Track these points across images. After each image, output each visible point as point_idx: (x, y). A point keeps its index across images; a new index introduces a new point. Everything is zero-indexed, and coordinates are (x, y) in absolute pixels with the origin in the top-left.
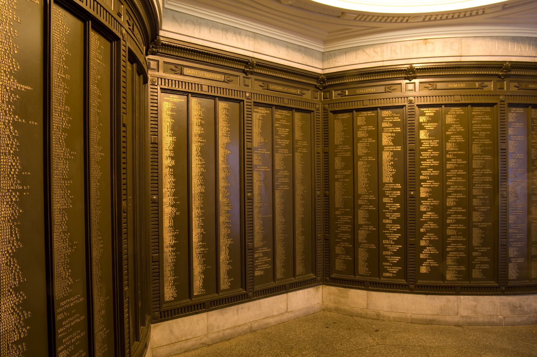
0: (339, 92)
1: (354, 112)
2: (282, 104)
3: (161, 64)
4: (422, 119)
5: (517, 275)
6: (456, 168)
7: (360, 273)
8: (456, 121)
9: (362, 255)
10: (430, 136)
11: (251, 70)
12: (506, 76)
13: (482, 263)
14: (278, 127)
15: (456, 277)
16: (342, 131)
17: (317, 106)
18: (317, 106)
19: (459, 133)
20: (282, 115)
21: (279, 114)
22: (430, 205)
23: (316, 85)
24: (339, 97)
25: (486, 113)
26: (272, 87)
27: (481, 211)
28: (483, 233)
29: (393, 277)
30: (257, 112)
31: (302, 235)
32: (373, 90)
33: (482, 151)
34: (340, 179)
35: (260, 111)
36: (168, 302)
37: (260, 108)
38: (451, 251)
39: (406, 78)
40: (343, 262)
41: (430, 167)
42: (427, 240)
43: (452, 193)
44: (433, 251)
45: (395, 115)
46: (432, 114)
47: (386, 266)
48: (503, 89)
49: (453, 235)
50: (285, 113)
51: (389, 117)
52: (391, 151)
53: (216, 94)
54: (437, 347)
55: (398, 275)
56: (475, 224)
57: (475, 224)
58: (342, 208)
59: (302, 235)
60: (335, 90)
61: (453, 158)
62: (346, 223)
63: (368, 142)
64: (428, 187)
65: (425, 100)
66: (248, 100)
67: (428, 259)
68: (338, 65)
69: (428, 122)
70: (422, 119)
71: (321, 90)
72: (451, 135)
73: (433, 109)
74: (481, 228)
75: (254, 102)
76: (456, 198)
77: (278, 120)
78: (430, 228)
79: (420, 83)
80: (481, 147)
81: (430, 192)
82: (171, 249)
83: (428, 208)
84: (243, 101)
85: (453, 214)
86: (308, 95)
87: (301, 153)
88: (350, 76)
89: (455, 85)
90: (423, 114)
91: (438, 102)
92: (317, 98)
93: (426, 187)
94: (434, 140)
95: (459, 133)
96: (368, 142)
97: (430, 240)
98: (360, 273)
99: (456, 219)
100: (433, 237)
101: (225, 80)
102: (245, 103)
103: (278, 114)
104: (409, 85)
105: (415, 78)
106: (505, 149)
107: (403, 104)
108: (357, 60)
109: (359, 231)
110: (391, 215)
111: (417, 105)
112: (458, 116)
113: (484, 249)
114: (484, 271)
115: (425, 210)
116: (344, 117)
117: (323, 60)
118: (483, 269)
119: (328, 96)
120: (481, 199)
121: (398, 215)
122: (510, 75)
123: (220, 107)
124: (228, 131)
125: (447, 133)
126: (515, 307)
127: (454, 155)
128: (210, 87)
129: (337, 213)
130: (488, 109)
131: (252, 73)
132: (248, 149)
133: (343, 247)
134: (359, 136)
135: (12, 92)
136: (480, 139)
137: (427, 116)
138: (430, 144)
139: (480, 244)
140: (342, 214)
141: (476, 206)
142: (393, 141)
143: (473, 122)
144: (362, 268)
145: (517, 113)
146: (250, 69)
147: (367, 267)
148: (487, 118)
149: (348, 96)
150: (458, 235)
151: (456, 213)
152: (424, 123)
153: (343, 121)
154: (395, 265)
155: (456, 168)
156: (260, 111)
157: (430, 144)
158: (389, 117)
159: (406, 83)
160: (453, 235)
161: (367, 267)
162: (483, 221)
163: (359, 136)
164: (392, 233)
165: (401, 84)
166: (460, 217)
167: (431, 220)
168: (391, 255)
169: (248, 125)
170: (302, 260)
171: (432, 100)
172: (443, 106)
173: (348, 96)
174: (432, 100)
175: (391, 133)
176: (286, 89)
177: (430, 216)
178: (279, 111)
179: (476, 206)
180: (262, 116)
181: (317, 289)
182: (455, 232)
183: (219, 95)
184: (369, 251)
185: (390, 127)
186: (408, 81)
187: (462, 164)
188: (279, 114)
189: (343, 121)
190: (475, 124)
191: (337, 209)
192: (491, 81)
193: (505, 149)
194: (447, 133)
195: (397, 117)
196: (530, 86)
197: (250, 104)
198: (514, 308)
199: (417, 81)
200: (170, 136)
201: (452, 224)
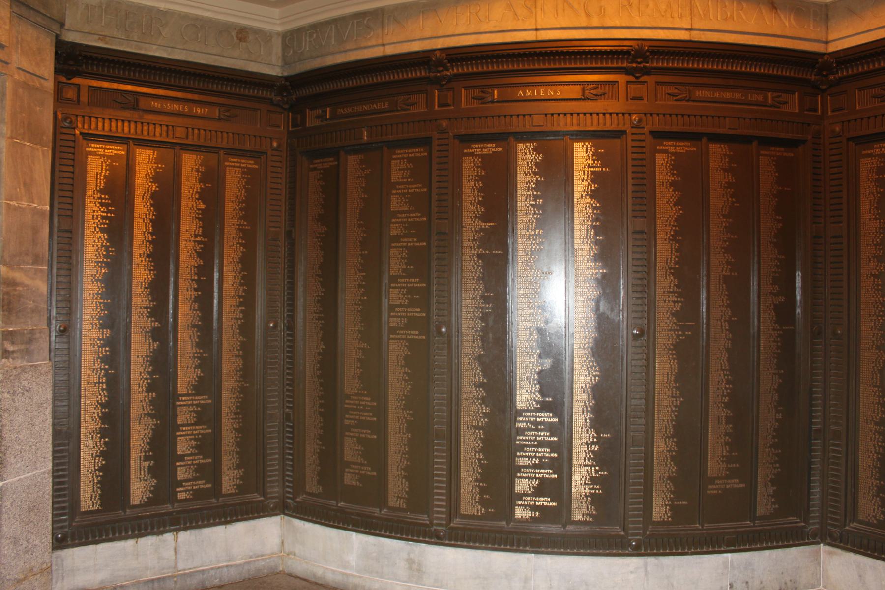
0: (477, 93)
7: (463, 512)
24: (476, 105)
32: (542, 93)
36: (135, 506)
48: (816, 110)
60: (466, 88)
82: (872, 426)
88: (483, 58)
89: (728, 95)
91: (614, 127)
98: (463, 512)
107: (623, 129)
119: (450, 101)
122: (841, 79)
131: (648, 72)
135: (476, 231)
149: (498, 102)
171: (595, 122)
173: (498, 102)
174: (601, 121)
192: (793, 93)
200: (876, 219)
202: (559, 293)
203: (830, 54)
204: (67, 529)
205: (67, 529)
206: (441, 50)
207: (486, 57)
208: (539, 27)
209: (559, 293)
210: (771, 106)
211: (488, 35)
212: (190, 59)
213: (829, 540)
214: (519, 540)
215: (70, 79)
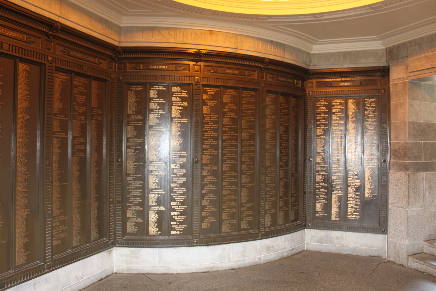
0: (133, 65)
1: (73, 74)
2: (81, 71)
3: (202, 67)
4: (205, 97)
5: (271, 223)
6: (230, 139)
8: (231, 101)
9: (153, 217)
10: (211, 111)
11: (54, 34)
12: (266, 69)
13: (248, 216)
14: (76, 94)
15: (230, 229)
16: (135, 102)
17: (112, 76)
18: (112, 76)
19: (233, 111)
20: (80, 82)
21: (78, 81)
22: (210, 170)
23: (112, 56)
25: (252, 96)
26: (73, 53)
27: (248, 175)
28: (249, 192)
29: (180, 234)
30: (57, 77)
31: (96, 201)
33: (248, 126)
34: (78, 144)
35: (60, 76)
37: (60, 73)
38: (226, 208)
39: (193, 61)
40: (134, 225)
41: (211, 138)
42: (207, 200)
43: (227, 160)
44: (213, 209)
45: (183, 91)
46: (213, 93)
47: (173, 225)
48: (263, 78)
49: (227, 195)
50: (83, 80)
51: (178, 92)
52: (179, 123)
53: (17, 55)
54: (222, 288)
55: (184, 232)
56: (243, 185)
57: (243, 185)
58: (134, 174)
59: (96, 201)
60: (129, 63)
61: (228, 131)
62: (137, 188)
63: (159, 114)
64: (209, 155)
65: (216, 81)
66: (49, 64)
67: (209, 216)
68: (135, 40)
69: (210, 99)
70: (205, 97)
71: (115, 61)
72: (227, 111)
73: (214, 89)
74: (247, 188)
75: (56, 67)
76: (230, 164)
77: (77, 86)
78: (210, 190)
79: (205, 66)
80: (248, 123)
81: (210, 159)
83: (209, 172)
84: (45, 64)
85: (227, 177)
86: (104, 65)
87: (96, 120)
90: (206, 93)
92: (112, 69)
93: (207, 155)
94: (215, 115)
95: (233, 111)
96: (159, 114)
97: (210, 200)
99: (229, 181)
100: (213, 197)
101: (28, 41)
102: (47, 67)
103: (77, 81)
104: (196, 66)
105: (201, 61)
106: (263, 125)
107: (191, 82)
108: (153, 39)
109: (150, 195)
110: (178, 180)
111: (202, 85)
112: (233, 97)
113: (249, 205)
114: (249, 223)
115: (206, 174)
116: (137, 89)
117: (120, 34)
118: (248, 221)
120: (248, 165)
121: (184, 179)
122: (268, 69)
123: (20, 69)
124: (28, 95)
125: (224, 110)
126: (269, 248)
127: (229, 128)
128: (11, 46)
129: (129, 178)
130: (253, 93)
131: (55, 37)
132: (48, 114)
133: (134, 210)
134: (150, 108)
136: (247, 116)
137: (209, 94)
138: (211, 118)
139: (247, 201)
140: (134, 180)
141: (244, 170)
142: (181, 114)
143: (243, 102)
144: (153, 229)
145: (271, 98)
146: (54, 32)
147: (157, 227)
148: (253, 100)
150: (231, 194)
151: (230, 176)
152: (206, 100)
153: (137, 93)
154: (181, 223)
155: (230, 139)
156: (60, 76)
157: (211, 118)
158: (178, 92)
159: (194, 65)
160: (227, 195)
161: (157, 227)
162: (249, 182)
163: (150, 108)
164: (179, 195)
165: (189, 65)
166: (233, 180)
167: (211, 183)
168: (178, 215)
169: (49, 90)
170: (96, 226)
172: (222, 88)
175: (179, 106)
176: (85, 57)
177: (210, 180)
178: (78, 78)
179: (244, 170)
180: (62, 82)
181: (110, 253)
182: (229, 192)
183: (20, 55)
184: (159, 213)
185: (179, 101)
186: (195, 63)
187: (234, 136)
188: (78, 81)
189: (137, 93)
190: (244, 104)
191: (128, 175)
193: (263, 125)
194: (224, 110)
195: (185, 93)
196: (279, 78)
197: (51, 68)
198: (269, 249)
199: (202, 64)
201: (227, 185)
202: (165, 146)
203: (121, 47)
204: (50, 263)
205: (50, 263)
206: (269, 59)
207: (147, 52)
208: (177, 42)
209: (165, 146)
210: (247, 76)
211: (207, 46)
212: (297, 64)
213: (117, 245)
214: (141, 243)
215: (197, 63)
